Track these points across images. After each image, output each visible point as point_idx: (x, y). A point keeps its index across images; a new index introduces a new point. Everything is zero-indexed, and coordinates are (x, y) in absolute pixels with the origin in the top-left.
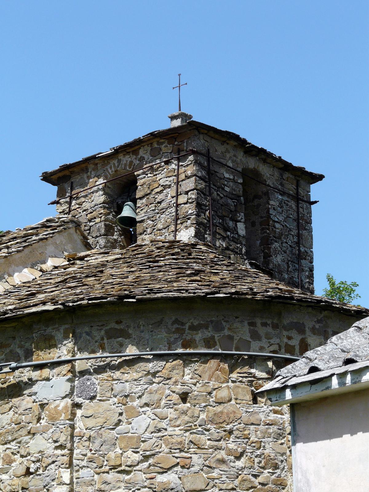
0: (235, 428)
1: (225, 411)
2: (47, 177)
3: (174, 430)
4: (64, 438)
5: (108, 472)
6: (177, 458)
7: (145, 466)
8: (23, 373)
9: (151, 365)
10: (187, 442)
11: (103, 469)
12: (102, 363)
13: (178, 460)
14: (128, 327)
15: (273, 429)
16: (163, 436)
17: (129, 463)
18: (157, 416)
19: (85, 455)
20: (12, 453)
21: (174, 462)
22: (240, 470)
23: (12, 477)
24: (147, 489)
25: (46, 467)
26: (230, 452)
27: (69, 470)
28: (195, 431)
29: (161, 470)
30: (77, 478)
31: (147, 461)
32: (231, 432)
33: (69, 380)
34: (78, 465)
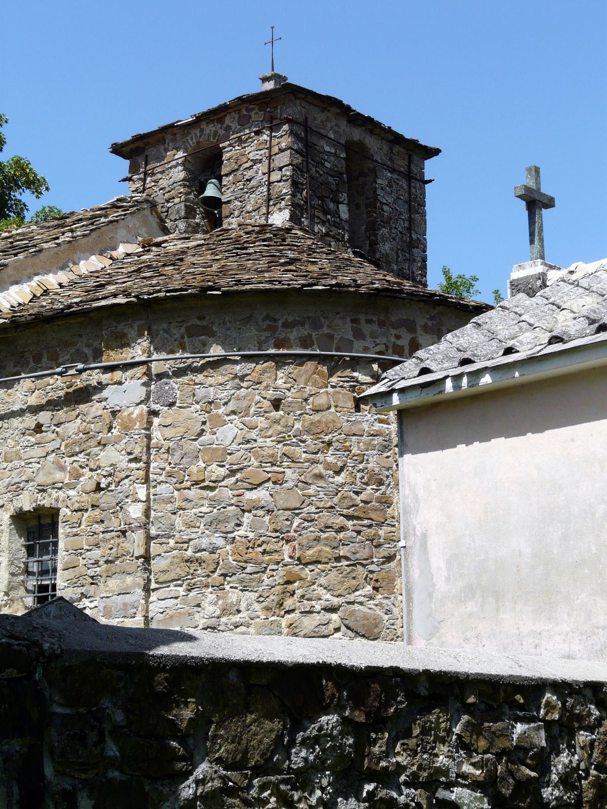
0: (334, 439)
2: (117, 149)
3: (265, 442)
4: (139, 450)
5: (189, 489)
6: (268, 472)
7: (232, 482)
8: (91, 376)
9: (238, 367)
10: (279, 455)
11: (184, 485)
12: (182, 365)
13: (269, 475)
14: (212, 323)
15: (378, 440)
17: (213, 478)
18: (245, 426)
19: (163, 469)
20: (80, 466)
21: (265, 477)
22: (340, 486)
24: (234, 507)
26: (328, 466)
27: (145, 485)
28: (288, 442)
29: (250, 486)
32: (329, 444)
33: (144, 384)
34: (156, 481)
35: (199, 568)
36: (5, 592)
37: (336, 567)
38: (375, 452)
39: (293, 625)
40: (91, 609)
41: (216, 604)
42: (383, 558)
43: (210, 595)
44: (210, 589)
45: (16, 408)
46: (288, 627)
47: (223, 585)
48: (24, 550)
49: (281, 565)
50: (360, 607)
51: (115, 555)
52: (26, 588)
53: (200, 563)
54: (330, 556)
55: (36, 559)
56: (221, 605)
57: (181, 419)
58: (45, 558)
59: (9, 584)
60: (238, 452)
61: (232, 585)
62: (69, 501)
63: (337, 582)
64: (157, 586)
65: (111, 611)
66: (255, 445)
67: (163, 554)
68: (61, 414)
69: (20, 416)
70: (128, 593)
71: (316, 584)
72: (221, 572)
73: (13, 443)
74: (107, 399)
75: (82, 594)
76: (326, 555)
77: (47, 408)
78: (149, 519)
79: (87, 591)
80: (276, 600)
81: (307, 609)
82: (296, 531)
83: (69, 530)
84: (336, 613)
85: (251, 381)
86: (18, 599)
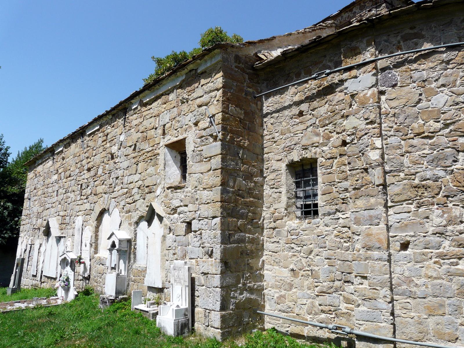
4: (374, 116)
5: (413, 138)
7: (447, 132)
8: (334, 78)
9: (445, 55)
11: (409, 136)
12: (400, 60)
17: (431, 130)
19: (392, 127)
20: (330, 132)
24: (450, 149)
27: (380, 138)
33: (374, 75)
34: (386, 135)
35: (425, 192)
40: (343, 219)
41: (442, 216)
43: (436, 211)
45: (286, 104)
47: (446, 203)
48: (294, 184)
51: (360, 184)
52: (296, 206)
53: (426, 188)
55: (301, 189)
56: (446, 217)
58: (307, 188)
59: (287, 204)
60: (450, 112)
61: (454, 203)
64: (393, 204)
65: (360, 221)
67: (396, 183)
68: (315, 104)
69: (289, 108)
70: (372, 209)
72: (444, 194)
73: (286, 124)
74: (347, 88)
75: (336, 209)
77: (306, 102)
83: (325, 171)
85: (456, 63)
86: (292, 213)
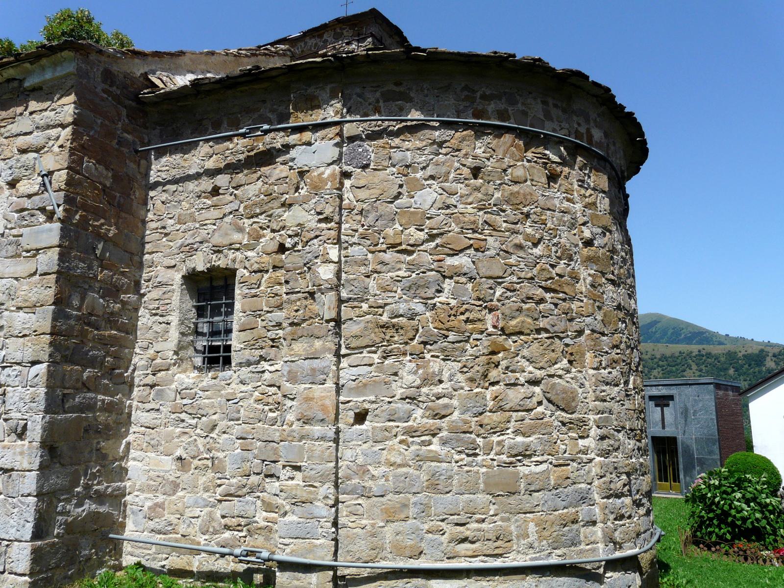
0: (532, 211)
1: (522, 191)
3: (466, 208)
4: (331, 210)
5: (385, 251)
6: (470, 239)
7: (432, 247)
8: (275, 139)
9: (437, 133)
10: (481, 222)
11: (379, 247)
12: (377, 128)
13: (471, 242)
14: (410, 89)
15: (567, 217)
16: (453, 214)
17: (411, 242)
18: (445, 191)
19: (356, 231)
20: (261, 228)
21: (467, 243)
22: (538, 258)
23: (261, 253)
24: (434, 273)
25: (307, 242)
26: (527, 237)
27: (337, 246)
28: (489, 210)
29: (452, 252)
30: (345, 257)
31: (433, 241)
32: (527, 215)
33: (337, 145)
34: (347, 242)
35: (395, 334)
36: (175, 351)
37: (537, 339)
38: (565, 228)
39: (499, 398)
40: (270, 372)
41: (415, 373)
42: (575, 332)
43: (409, 364)
44: (409, 358)
45: (192, 172)
46: (493, 400)
47: (423, 353)
48: (194, 310)
49: (485, 334)
50: (559, 380)
54: (532, 328)
55: (206, 320)
57: (377, 181)
58: (216, 319)
59: (179, 344)
61: (433, 354)
62: (247, 262)
63: (538, 354)
64: (348, 352)
65: (296, 377)
66: (456, 211)
67: (355, 319)
68: (241, 177)
69: (196, 179)
70: (316, 358)
71: (520, 356)
72: (421, 340)
73: (187, 206)
75: (261, 356)
76: (528, 326)
78: (340, 282)
79: (266, 353)
80: (481, 371)
81: (512, 382)
82: (499, 300)
83: (247, 291)
84: (538, 386)
86: (187, 359)
